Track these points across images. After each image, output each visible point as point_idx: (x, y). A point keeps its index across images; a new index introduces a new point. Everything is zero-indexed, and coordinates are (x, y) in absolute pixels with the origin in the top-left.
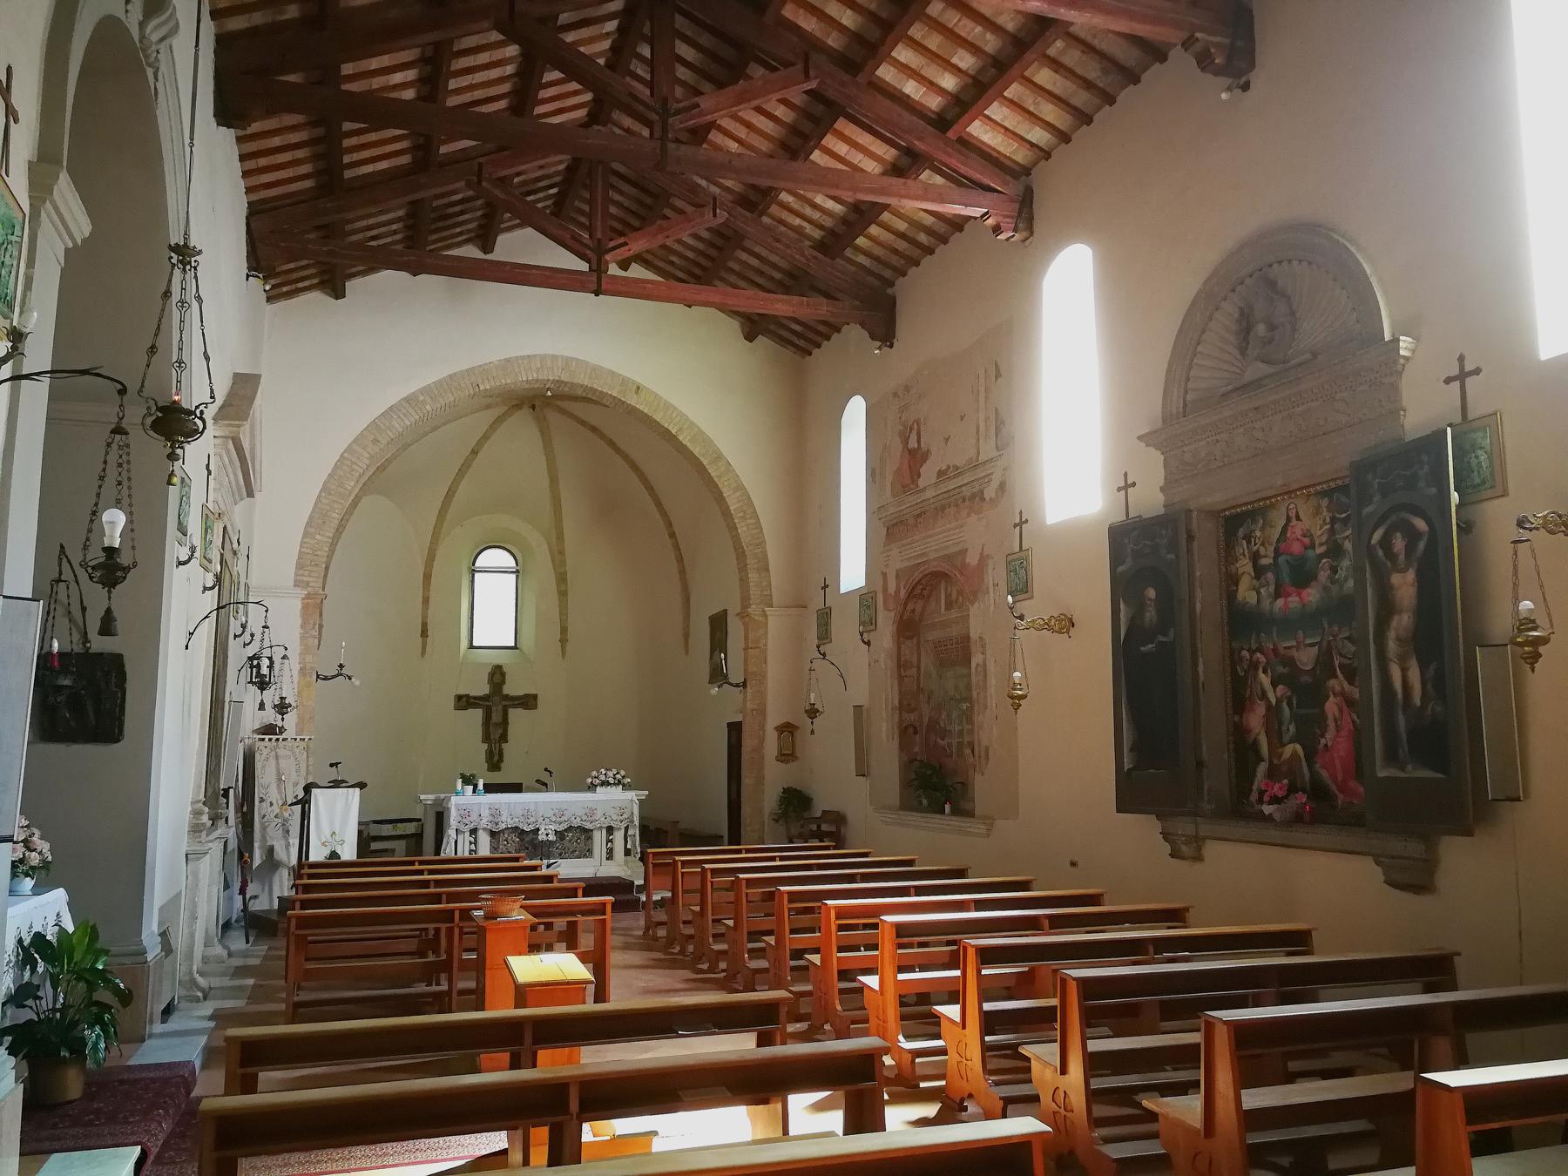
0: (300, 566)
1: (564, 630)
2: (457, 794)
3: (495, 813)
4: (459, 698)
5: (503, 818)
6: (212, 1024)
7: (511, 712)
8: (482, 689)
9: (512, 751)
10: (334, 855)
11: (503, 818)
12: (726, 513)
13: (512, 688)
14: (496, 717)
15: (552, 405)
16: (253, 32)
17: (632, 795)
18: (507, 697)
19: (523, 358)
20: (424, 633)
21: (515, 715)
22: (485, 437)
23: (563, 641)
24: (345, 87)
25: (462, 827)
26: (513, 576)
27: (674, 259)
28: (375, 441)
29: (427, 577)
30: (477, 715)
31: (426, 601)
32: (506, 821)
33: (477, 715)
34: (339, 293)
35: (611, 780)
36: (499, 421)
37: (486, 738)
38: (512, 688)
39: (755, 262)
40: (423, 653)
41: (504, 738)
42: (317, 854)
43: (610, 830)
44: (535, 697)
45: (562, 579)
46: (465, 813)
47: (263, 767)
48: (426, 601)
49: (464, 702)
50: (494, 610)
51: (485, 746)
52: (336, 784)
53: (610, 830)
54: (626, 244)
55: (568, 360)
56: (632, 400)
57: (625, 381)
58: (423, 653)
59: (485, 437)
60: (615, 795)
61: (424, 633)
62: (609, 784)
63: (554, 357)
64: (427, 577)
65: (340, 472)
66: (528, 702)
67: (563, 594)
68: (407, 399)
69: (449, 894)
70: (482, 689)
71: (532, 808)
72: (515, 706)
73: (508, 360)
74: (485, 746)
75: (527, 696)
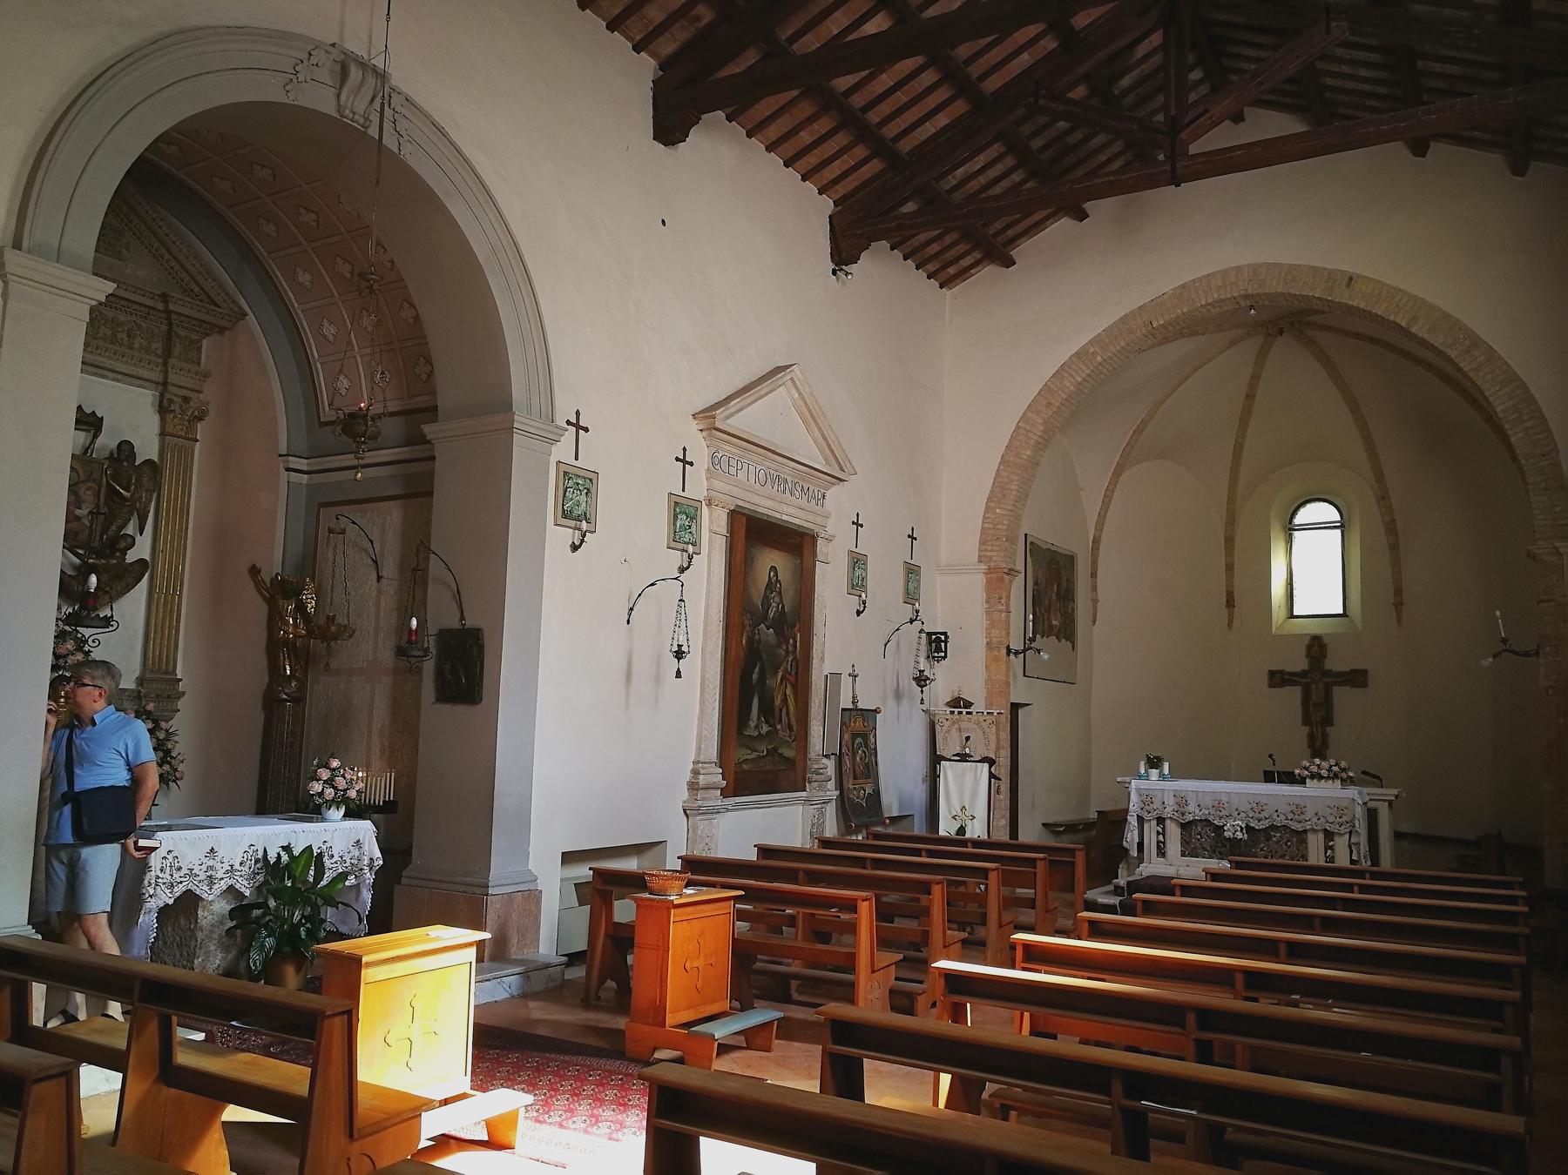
0: (983, 542)
1: (1398, 592)
2: (1140, 777)
3: (1182, 802)
4: (1272, 674)
5: (1191, 808)
6: (565, 959)
7: (1297, 690)
8: (1299, 663)
9: (1339, 734)
10: (962, 830)
11: (1191, 808)
12: (1491, 419)
13: (1335, 663)
14: (1317, 696)
15: (1288, 321)
16: (686, 48)
17: (1352, 792)
18: (1329, 673)
19: (1201, 279)
20: (1230, 603)
21: (1341, 694)
22: (1255, 378)
23: (1398, 605)
24: (920, 60)
25: (1146, 816)
26: (1338, 532)
27: (1372, 103)
28: (1049, 404)
29: (1229, 541)
30: (1294, 694)
31: (1230, 568)
32: (1193, 812)
33: (1294, 694)
34: (1009, 262)
35: (1324, 773)
36: (1262, 356)
37: (1306, 720)
38: (1335, 663)
39: (1453, 69)
40: (1230, 624)
41: (1328, 720)
42: (946, 828)
43: (1329, 836)
44: (1364, 673)
45: (1391, 529)
46: (1147, 799)
47: (945, 739)
48: (1230, 568)
49: (1278, 679)
50: (1313, 571)
51: (1306, 730)
52: (963, 758)
53: (1329, 836)
54: (1207, 111)
55: (1254, 268)
56: (1343, 296)
57: (1331, 274)
58: (1230, 624)
59: (1255, 378)
60: (1329, 791)
61: (1230, 603)
62: (1321, 777)
63: (1238, 269)
64: (1229, 541)
65: (1016, 443)
66: (1357, 678)
67: (1394, 548)
68: (1077, 354)
69: (809, 873)
70: (1299, 663)
71: (1224, 799)
72: (1341, 684)
73: (1183, 286)
74: (1306, 730)
75: (1354, 671)
